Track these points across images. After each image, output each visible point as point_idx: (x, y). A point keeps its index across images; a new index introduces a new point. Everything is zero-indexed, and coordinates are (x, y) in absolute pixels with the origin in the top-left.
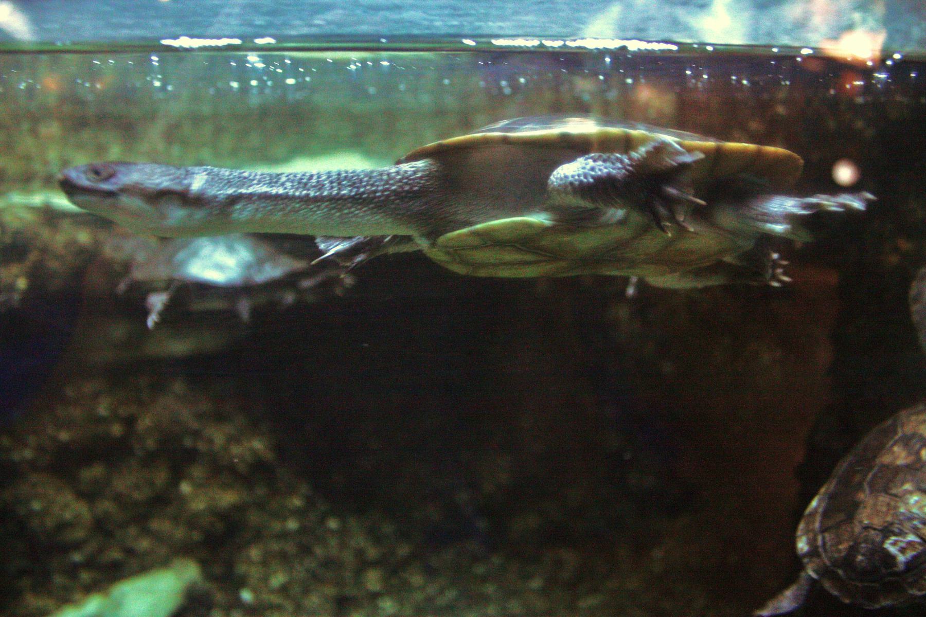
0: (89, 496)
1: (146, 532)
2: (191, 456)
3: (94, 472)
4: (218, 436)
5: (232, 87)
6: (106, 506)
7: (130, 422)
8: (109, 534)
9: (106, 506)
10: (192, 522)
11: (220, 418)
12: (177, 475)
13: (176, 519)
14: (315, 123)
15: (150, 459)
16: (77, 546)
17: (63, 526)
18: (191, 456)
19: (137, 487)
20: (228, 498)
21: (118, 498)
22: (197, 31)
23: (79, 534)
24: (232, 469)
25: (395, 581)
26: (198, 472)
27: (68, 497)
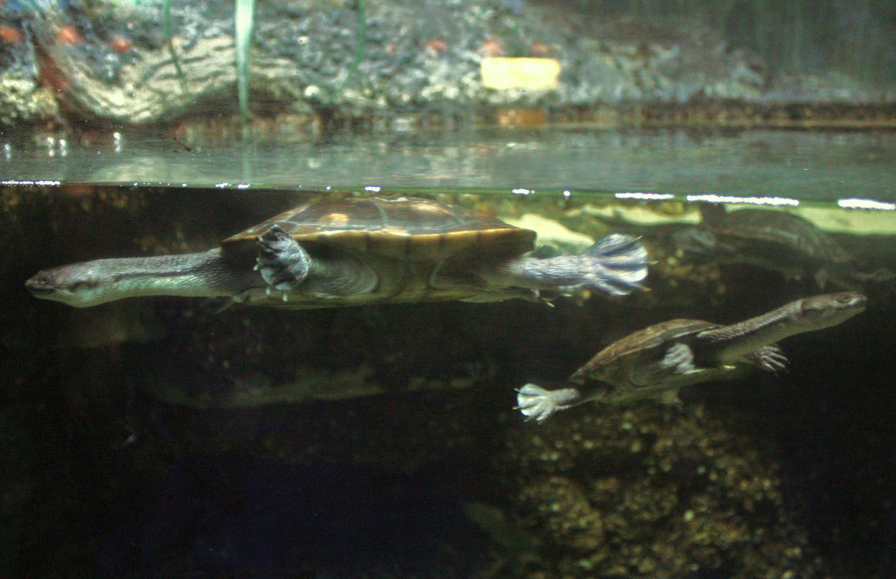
0: (603, 507)
1: (648, 553)
2: (700, 485)
3: (607, 485)
4: (730, 467)
5: (549, 383)
6: (616, 520)
7: (649, 440)
8: (615, 548)
9: (616, 520)
10: (691, 552)
11: (735, 451)
12: (684, 503)
13: (676, 544)
14: (689, 268)
15: (661, 481)
16: (588, 554)
17: (577, 531)
18: (700, 485)
19: (647, 508)
20: (731, 536)
21: (627, 514)
22: (646, 189)
23: (592, 543)
24: (739, 506)
25: (301, 269)
26: (704, 502)
27: (581, 505)
